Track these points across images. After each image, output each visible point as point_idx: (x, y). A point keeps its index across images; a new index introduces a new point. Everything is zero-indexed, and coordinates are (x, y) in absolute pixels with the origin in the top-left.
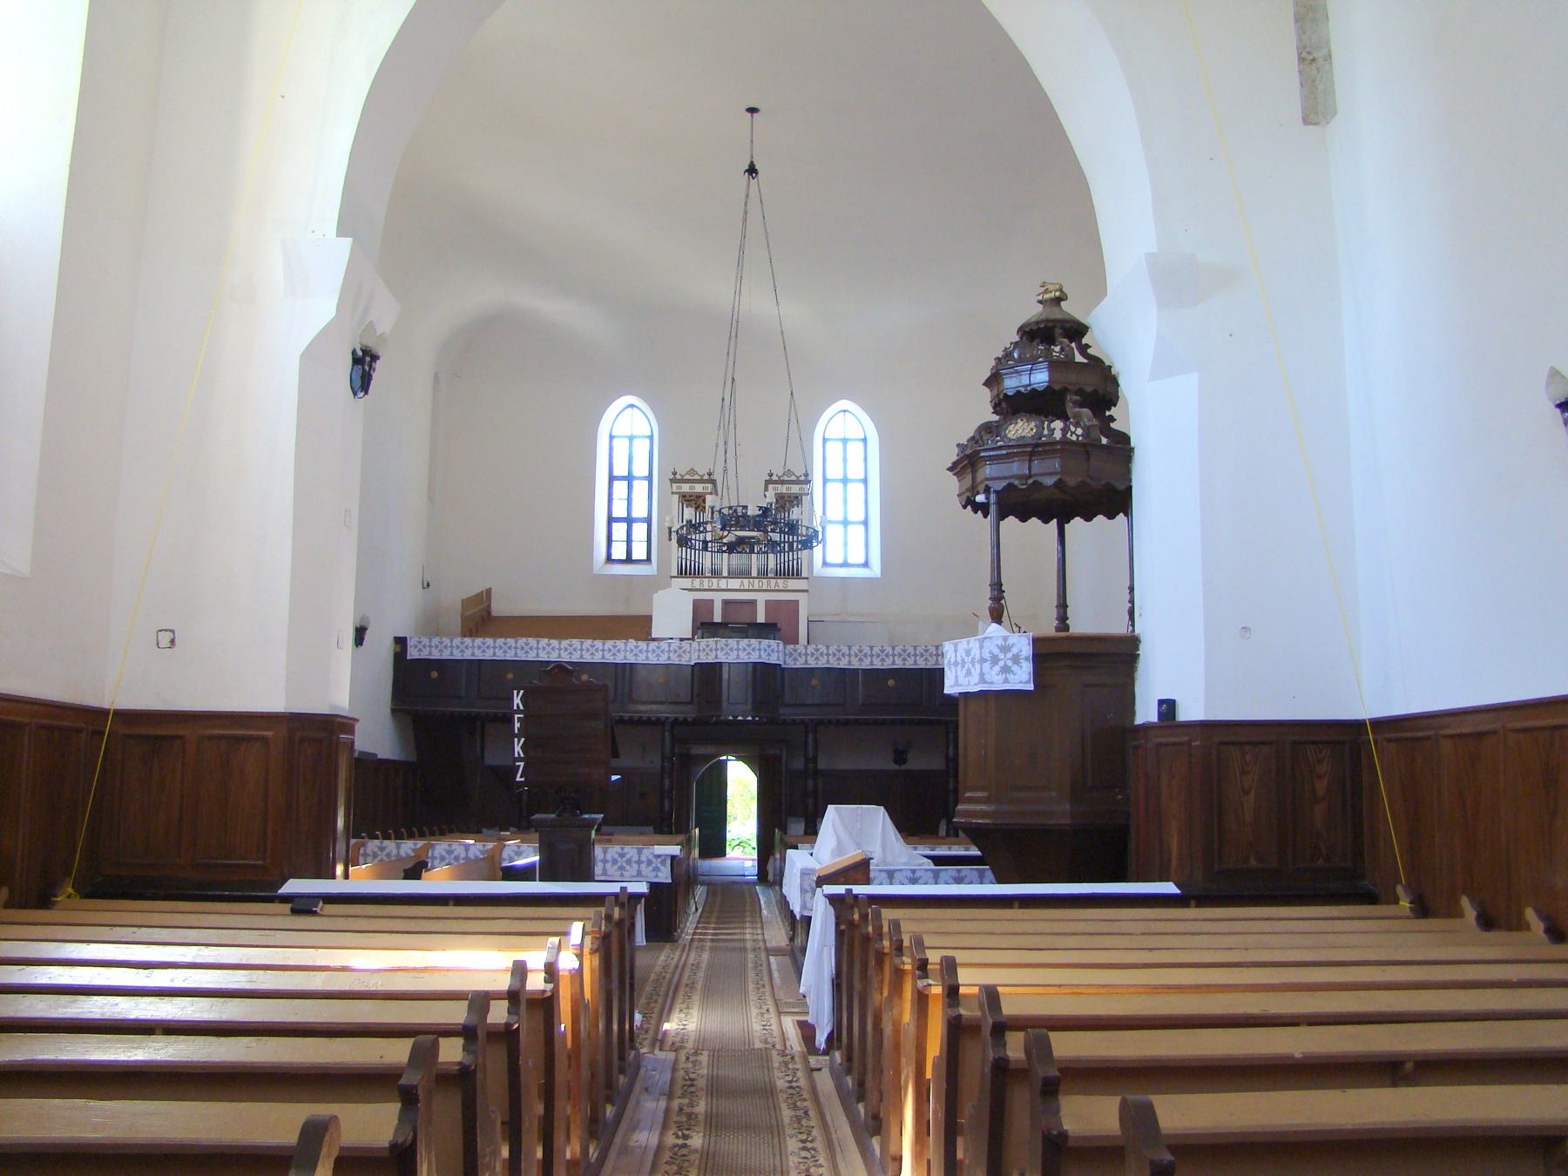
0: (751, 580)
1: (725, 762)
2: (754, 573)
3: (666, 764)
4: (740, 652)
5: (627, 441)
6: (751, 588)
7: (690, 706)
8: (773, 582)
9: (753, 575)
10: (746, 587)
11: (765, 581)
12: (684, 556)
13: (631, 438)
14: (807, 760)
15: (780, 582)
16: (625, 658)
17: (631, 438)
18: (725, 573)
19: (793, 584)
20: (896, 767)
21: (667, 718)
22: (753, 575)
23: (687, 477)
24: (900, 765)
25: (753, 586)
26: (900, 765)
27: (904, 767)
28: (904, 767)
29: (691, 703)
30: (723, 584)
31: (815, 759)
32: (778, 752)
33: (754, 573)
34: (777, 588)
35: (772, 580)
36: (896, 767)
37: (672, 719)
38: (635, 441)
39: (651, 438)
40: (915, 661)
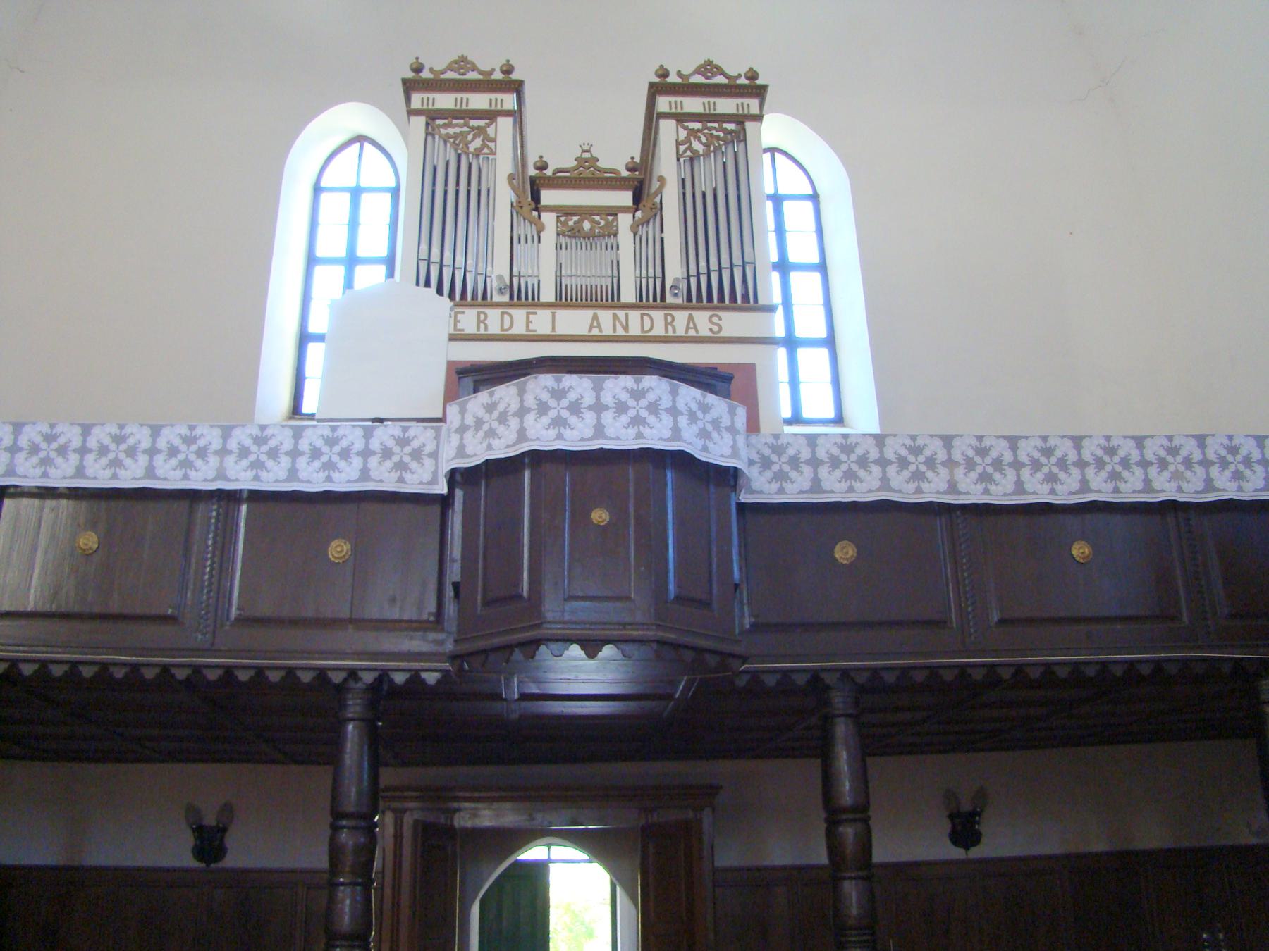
0: (621, 314)
1: (538, 872)
2: (628, 295)
3: (344, 836)
4: (608, 417)
5: (347, 197)
6: (620, 332)
7: (432, 636)
8: (681, 317)
9: (624, 299)
10: (608, 331)
11: (658, 315)
12: (435, 257)
13: (356, 193)
14: (834, 816)
15: (702, 318)
16: (221, 475)
18: (548, 295)
19: (734, 323)
20: (957, 853)
21: (353, 674)
22: (624, 299)
23: (451, 75)
24: (967, 848)
25: (626, 328)
26: (967, 848)
27: (975, 853)
28: (975, 853)
29: (439, 618)
30: (542, 321)
31: (861, 812)
32: (691, 814)
33: (628, 295)
34: (692, 333)
35: (677, 314)
36: (957, 853)
37: (368, 678)
38: (365, 197)
39: (395, 192)
40: (1147, 481)
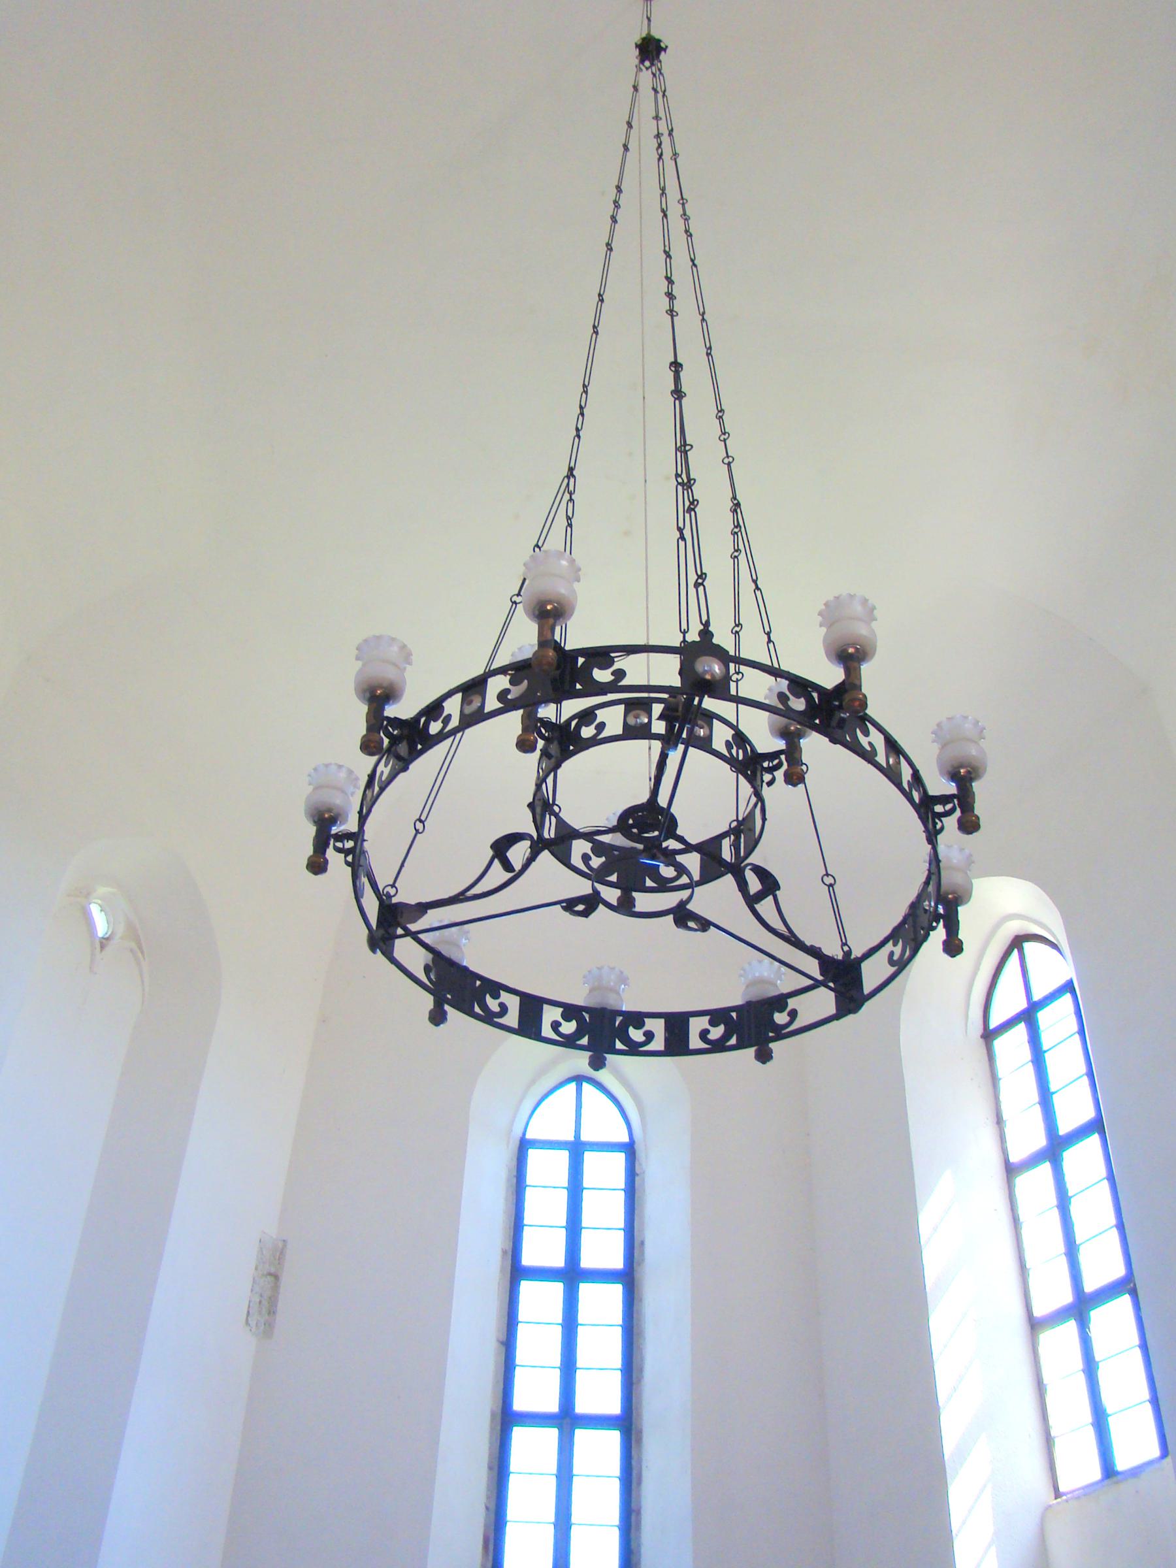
5: (564, 1156)
13: (577, 1149)
17: (577, 1149)
